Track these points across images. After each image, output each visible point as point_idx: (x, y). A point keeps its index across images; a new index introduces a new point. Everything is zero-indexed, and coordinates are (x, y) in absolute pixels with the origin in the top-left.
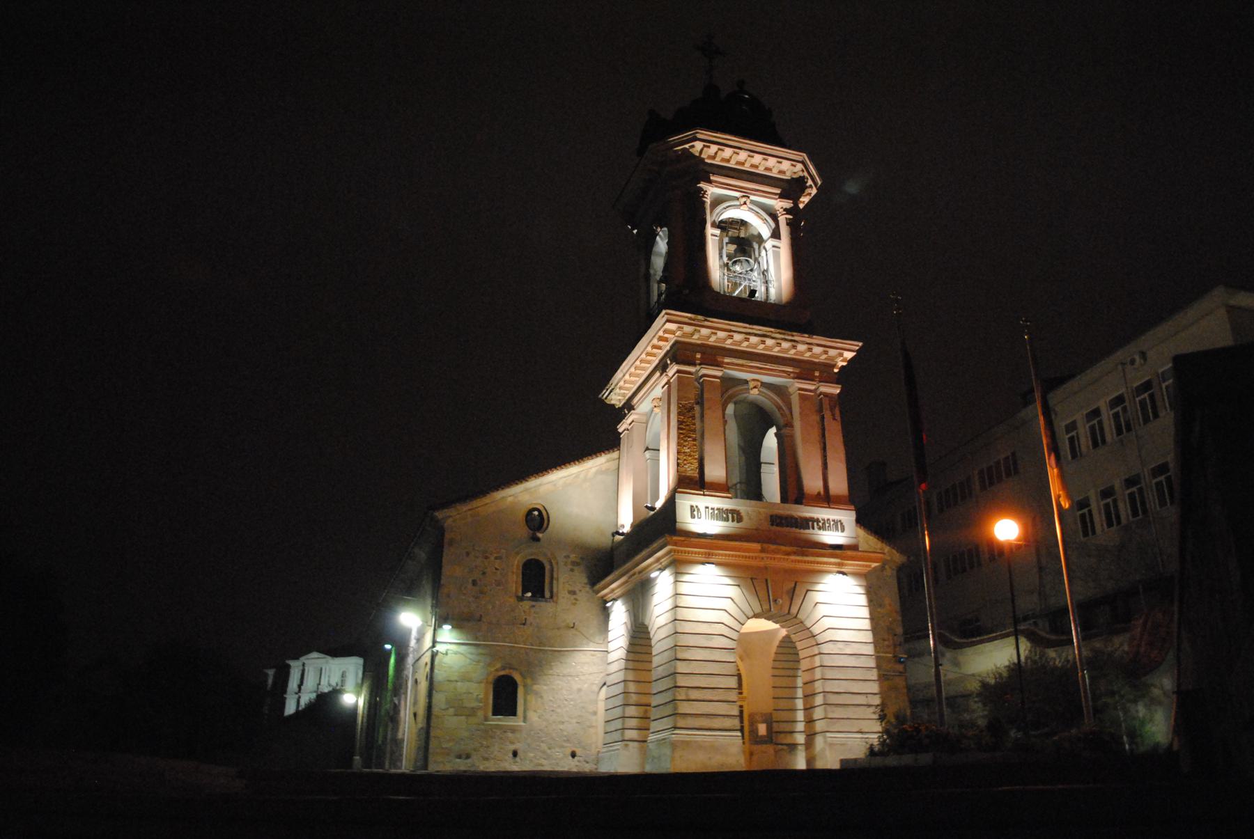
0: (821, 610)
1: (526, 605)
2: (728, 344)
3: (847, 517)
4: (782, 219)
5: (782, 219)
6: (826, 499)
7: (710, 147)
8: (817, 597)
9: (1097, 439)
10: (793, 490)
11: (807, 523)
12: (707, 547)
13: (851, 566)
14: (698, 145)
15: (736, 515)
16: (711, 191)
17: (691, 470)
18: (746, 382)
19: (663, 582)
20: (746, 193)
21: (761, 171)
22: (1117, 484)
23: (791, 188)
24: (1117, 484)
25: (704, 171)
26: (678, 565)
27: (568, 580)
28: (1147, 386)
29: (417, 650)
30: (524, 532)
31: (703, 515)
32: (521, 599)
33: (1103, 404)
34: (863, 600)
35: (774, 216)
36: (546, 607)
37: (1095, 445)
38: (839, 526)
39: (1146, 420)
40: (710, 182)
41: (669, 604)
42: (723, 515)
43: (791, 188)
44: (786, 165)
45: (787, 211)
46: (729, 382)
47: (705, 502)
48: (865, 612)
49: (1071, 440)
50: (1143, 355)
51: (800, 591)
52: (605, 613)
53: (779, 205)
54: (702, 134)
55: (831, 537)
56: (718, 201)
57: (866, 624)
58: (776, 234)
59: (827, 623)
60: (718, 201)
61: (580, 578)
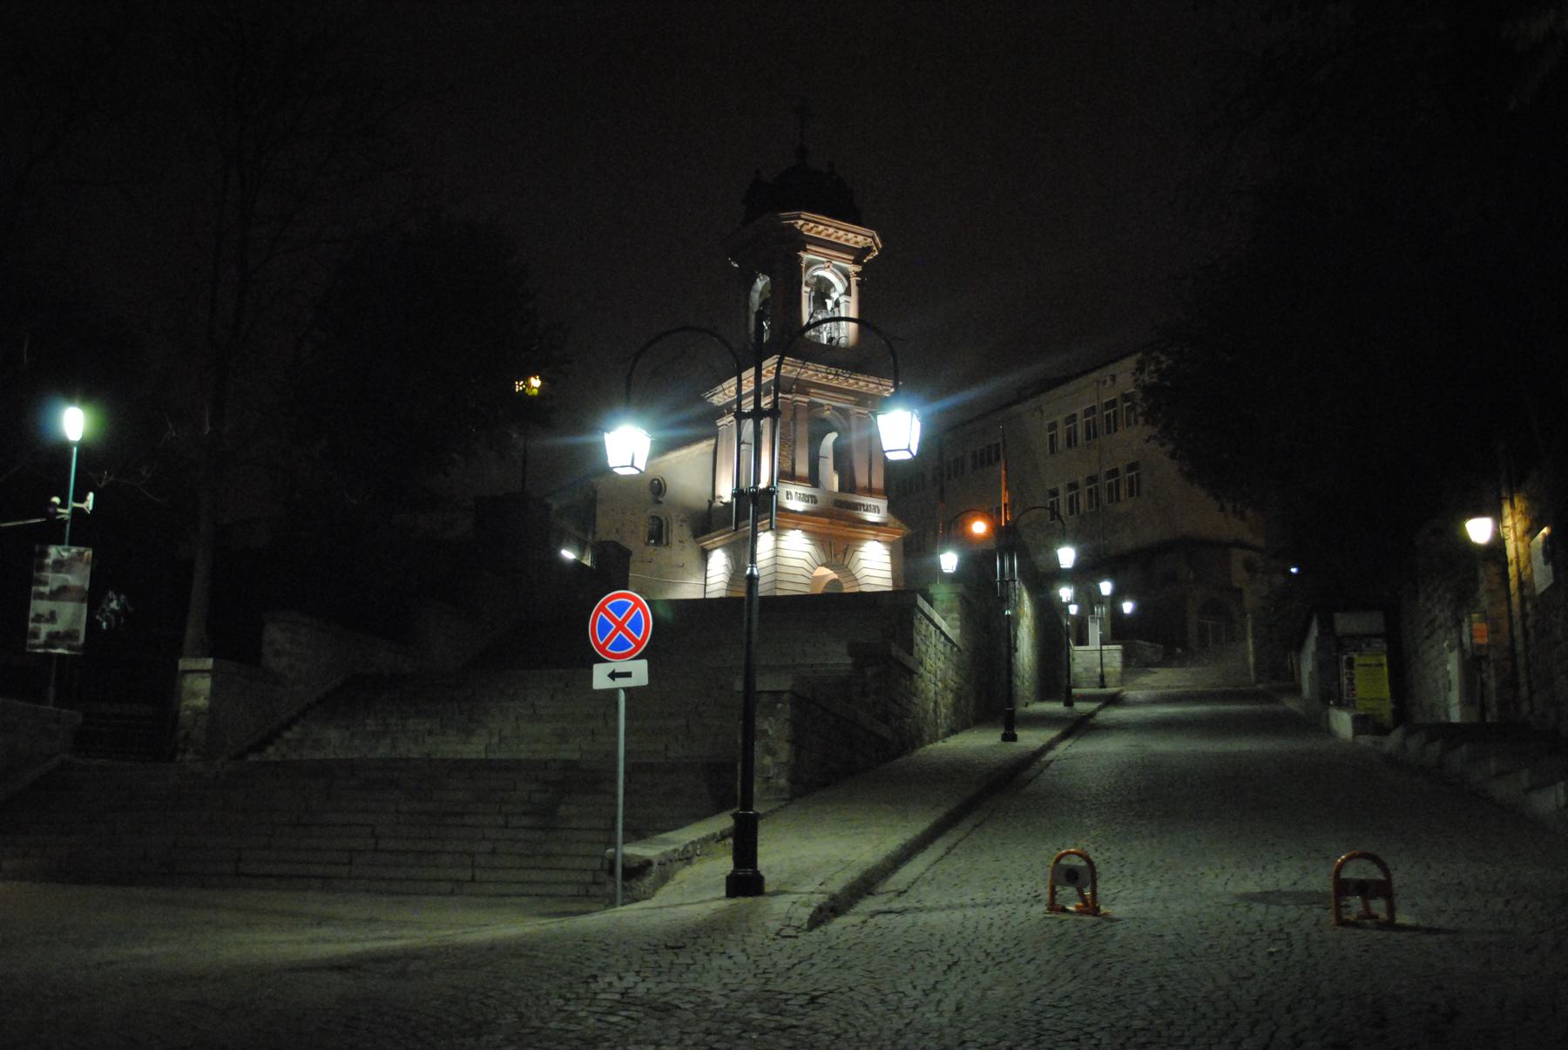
0: (863, 564)
1: (651, 549)
2: (814, 379)
3: (882, 504)
4: (854, 280)
5: (854, 280)
6: (870, 491)
7: (812, 225)
8: (861, 555)
9: (1071, 441)
10: (848, 484)
11: (857, 506)
12: (796, 519)
13: (883, 536)
14: (801, 222)
15: (813, 499)
16: (806, 257)
17: (787, 467)
18: (822, 405)
19: (765, 541)
20: (830, 258)
21: (842, 241)
22: (1081, 480)
23: (859, 255)
24: (1081, 480)
25: (802, 242)
26: (778, 531)
27: (679, 532)
28: (1112, 404)
29: (1518, 517)
30: (648, 496)
31: (794, 498)
32: (647, 544)
33: (1079, 412)
34: (888, 559)
35: (848, 277)
36: (665, 551)
37: (1069, 445)
38: (876, 509)
39: (1109, 432)
40: (806, 250)
41: (770, 554)
42: (805, 498)
43: (859, 255)
44: (860, 238)
45: (858, 274)
46: (812, 405)
47: (797, 489)
48: (889, 567)
49: (1052, 437)
50: (1113, 378)
51: (850, 551)
52: (705, 555)
53: (853, 268)
54: (805, 215)
55: (872, 517)
56: (811, 264)
57: (889, 575)
58: (848, 292)
59: (866, 572)
60: (811, 264)
61: (686, 532)
